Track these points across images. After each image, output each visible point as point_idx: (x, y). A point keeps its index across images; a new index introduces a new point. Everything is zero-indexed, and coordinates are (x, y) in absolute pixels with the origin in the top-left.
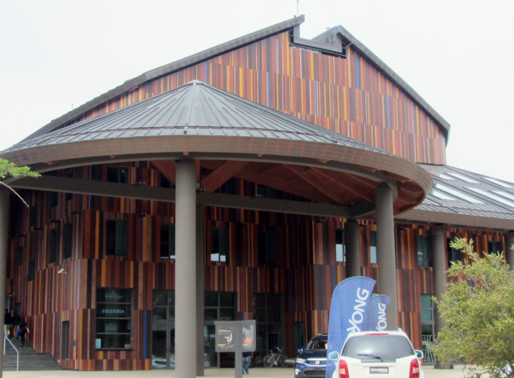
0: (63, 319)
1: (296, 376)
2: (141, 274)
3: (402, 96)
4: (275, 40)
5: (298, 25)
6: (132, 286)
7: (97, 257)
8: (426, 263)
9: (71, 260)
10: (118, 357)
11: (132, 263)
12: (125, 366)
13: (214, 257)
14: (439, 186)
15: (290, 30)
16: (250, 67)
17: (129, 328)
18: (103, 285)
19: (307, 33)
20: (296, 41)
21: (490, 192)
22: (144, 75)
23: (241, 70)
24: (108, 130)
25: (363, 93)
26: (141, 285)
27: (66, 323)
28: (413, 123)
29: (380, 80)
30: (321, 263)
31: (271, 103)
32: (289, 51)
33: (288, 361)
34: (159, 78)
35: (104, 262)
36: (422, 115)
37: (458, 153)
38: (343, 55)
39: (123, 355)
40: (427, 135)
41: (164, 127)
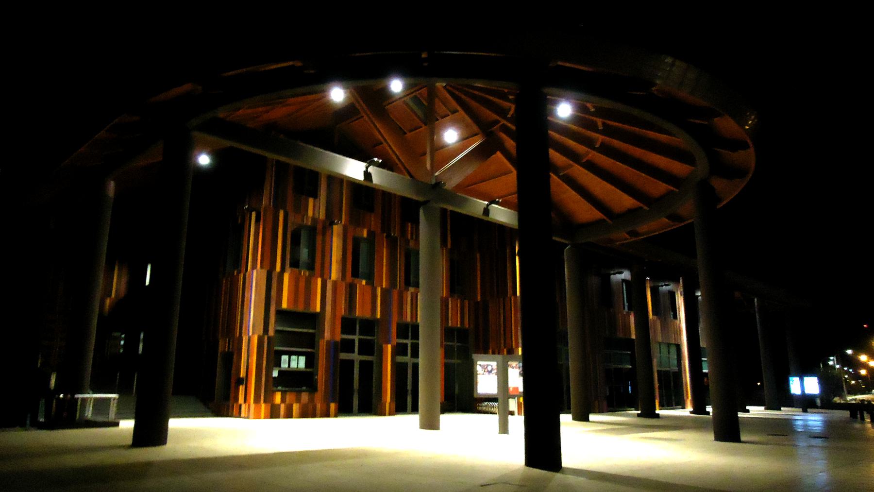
1: (873, 427)
7: (278, 269)
9: (239, 272)
11: (319, 281)
12: (306, 413)
18: (285, 305)
26: (328, 308)
28: (652, 134)
33: (837, 400)
35: (286, 277)
39: (305, 397)
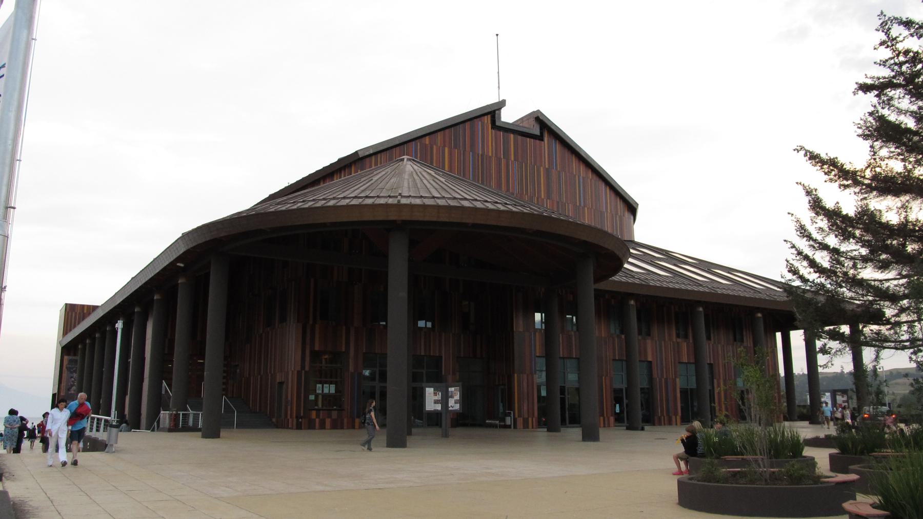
0: (278, 381)
2: (352, 339)
3: (595, 177)
4: (479, 124)
5: (500, 109)
6: (343, 350)
8: (618, 332)
10: (330, 416)
13: (421, 324)
14: (630, 260)
15: (492, 113)
16: (455, 148)
17: (646, 428)
18: (317, 348)
19: (508, 116)
20: (497, 124)
21: (675, 265)
22: (356, 152)
23: (446, 149)
24: (324, 199)
25: (559, 172)
27: (281, 383)
29: (574, 162)
30: (521, 330)
31: (506, 143)
32: (490, 132)
34: (370, 155)
35: (317, 327)
36: (613, 195)
37: (645, 231)
38: (540, 138)
40: (617, 214)
41: (378, 197)
